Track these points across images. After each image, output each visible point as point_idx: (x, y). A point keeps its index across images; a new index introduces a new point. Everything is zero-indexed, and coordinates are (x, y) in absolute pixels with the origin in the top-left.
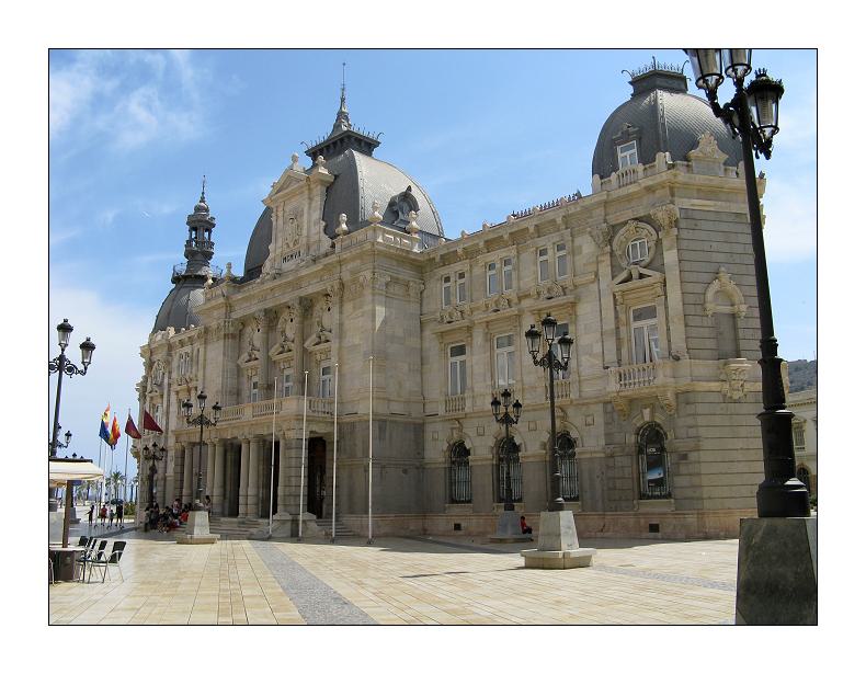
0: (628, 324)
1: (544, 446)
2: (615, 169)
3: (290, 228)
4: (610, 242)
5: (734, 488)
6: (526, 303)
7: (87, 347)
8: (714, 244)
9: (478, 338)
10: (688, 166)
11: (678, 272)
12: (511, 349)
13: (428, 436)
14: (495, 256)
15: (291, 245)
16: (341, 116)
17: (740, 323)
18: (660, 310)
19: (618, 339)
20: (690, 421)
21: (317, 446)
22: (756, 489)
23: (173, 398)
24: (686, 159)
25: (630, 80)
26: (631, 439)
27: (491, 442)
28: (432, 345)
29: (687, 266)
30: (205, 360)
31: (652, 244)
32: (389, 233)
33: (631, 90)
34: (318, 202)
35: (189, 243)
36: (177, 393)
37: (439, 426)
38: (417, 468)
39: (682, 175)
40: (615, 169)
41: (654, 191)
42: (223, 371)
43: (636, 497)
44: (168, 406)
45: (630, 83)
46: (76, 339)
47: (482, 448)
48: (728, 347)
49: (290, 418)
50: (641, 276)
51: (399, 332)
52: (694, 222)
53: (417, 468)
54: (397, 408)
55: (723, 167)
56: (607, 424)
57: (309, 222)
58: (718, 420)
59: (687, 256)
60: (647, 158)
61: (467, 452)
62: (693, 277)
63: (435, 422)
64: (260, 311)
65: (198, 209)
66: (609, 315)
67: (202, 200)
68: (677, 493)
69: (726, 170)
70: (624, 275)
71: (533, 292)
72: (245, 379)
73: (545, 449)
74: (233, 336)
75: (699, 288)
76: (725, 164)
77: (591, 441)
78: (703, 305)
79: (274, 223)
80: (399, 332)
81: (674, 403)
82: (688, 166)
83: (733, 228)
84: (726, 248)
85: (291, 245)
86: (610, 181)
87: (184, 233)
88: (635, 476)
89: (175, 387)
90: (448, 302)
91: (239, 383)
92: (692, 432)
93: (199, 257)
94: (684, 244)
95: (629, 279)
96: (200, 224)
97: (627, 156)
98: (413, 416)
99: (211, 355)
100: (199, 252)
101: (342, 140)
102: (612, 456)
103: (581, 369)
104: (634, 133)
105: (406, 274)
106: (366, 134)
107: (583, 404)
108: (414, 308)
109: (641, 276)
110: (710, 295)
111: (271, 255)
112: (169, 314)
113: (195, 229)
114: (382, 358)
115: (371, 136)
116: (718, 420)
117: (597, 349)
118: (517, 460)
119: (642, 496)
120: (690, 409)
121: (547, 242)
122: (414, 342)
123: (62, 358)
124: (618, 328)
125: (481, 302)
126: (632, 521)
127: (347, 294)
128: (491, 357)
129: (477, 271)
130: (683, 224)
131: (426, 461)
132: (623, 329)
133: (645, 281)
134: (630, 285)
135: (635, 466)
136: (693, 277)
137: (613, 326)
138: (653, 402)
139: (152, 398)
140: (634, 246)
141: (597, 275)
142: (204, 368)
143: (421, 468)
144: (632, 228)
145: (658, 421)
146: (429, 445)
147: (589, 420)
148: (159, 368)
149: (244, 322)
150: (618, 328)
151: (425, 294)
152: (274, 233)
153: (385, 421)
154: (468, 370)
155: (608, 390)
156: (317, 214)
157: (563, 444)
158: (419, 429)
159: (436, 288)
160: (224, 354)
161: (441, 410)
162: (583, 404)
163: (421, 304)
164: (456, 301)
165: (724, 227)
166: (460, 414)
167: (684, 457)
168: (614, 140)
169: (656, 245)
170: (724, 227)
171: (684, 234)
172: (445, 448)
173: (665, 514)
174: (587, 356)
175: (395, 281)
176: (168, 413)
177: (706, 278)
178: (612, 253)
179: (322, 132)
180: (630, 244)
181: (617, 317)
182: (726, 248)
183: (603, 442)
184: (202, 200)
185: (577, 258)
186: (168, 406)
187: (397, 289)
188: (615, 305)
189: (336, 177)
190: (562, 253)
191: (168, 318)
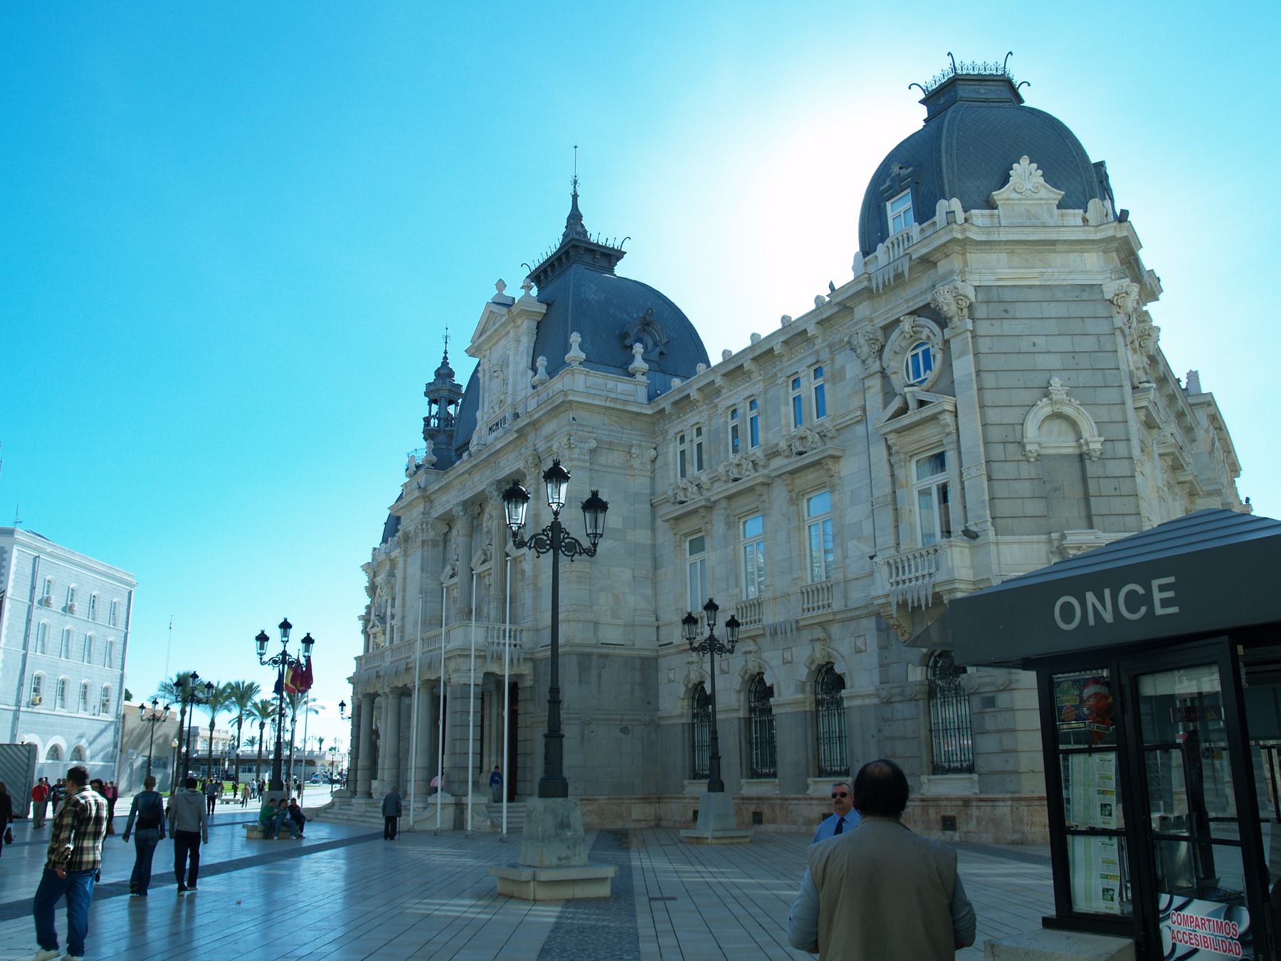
4: (881, 357)
6: (776, 463)
7: (308, 641)
8: (1039, 341)
13: (662, 677)
15: (497, 410)
16: (575, 217)
17: (1091, 469)
22: (911, 796)
24: (991, 205)
25: (923, 96)
27: (803, 673)
30: (405, 579)
33: (923, 112)
35: (427, 420)
41: (935, 264)
45: (922, 102)
46: (296, 635)
47: (791, 692)
50: (922, 403)
56: (882, 648)
61: (769, 692)
63: (669, 655)
64: (458, 504)
66: (882, 471)
70: (896, 404)
73: (803, 692)
75: (1011, 416)
76: (1059, 207)
84: (1064, 343)
85: (497, 410)
90: (683, 474)
95: (904, 410)
97: (899, 209)
98: (638, 645)
102: (888, 702)
104: (909, 175)
106: (602, 242)
107: (851, 619)
109: (922, 403)
110: (1031, 431)
111: (479, 423)
113: (435, 402)
115: (610, 244)
117: (867, 529)
118: (839, 703)
122: (642, 536)
123: (284, 653)
130: (981, 312)
131: (660, 714)
133: (927, 412)
134: (905, 420)
141: (864, 409)
142: (404, 590)
143: (655, 724)
146: (663, 691)
147: (860, 643)
148: (383, 593)
149: (448, 520)
151: (659, 463)
153: (589, 655)
155: (874, 594)
160: (422, 569)
162: (851, 619)
163: (653, 479)
164: (692, 470)
167: (990, 702)
171: (983, 328)
174: (854, 542)
177: (1026, 397)
178: (883, 372)
182: (1064, 343)
183: (876, 679)
189: (549, 305)
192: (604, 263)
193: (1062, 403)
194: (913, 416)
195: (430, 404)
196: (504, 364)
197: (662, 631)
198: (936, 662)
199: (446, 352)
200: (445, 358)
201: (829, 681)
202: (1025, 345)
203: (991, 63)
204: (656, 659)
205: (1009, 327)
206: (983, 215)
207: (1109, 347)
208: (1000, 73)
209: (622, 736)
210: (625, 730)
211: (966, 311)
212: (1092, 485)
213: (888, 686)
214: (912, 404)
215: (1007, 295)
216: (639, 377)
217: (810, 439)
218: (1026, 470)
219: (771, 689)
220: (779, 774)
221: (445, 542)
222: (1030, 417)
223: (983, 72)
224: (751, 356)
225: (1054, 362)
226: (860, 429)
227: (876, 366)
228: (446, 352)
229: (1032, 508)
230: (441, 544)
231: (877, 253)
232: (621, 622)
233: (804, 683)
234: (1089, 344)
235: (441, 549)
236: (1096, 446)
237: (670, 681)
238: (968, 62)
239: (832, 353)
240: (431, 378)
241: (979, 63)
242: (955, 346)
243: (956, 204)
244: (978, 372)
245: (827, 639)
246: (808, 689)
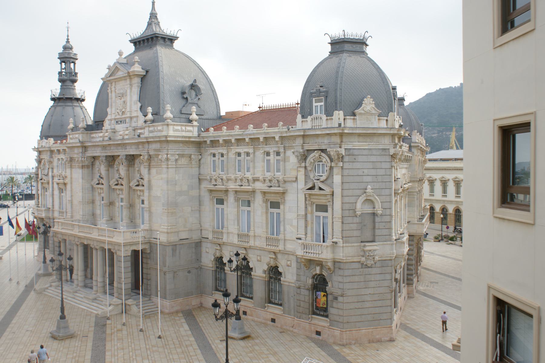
0: (312, 213)
1: (265, 272)
2: (311, 114)
3: (119, 102)
4: (305, 159)
5: (378, 286)
8: (366, 171)
9: (231, 198)
10: (354, 119)
11: (340, 190)
12: (248, 209)
13: (204, 249)
14: (242, 149)
16: (153, 16)
17: (377, 219)
18: (330, 209)
19: (306, 221)
20: (340, 279)
21: (135, 253)
23: (56, 186)
24: (354, 114)
25: (330, 41)
26: (310, 281)
28: (206, 197)
29: (346, 186)
31: (328, 168)
32: (177, 125)
33: (329, 48)
34: (136, 90)
35: (60, 73)
36: (58, 184)
37: (209, 245)
38: (197, 269)
39: (350, 123)
40: (311, 114)
42: (82, 189)
43: (311, 313)
44: (53, 191)
48: (368, 235)
49: (122, 238)
51: (185, 188)
52: (354, 157)
53: (197, 269)
54: (184, 235)
55: (377, 118)
57: (131, 100)
58: (356, 279)
59: (346, 179)
60: (329, 113)
62: (350, 193)
65: (65, 48)
67: (68, 41)
68: (330, 316)
69: (379, 119)
70: (310, 185)
71: (261, 178)
72: (97, 194)
73: (265, 274)
74: (88, 167)
75: (352, 200)
77: (289, 276)
78: (354, 211)
79: (110, 95)
80: (185, 188)
81: (332, 268)
82: (354, 119)
83: (379, 159)
84: (373, 172)
86: (307, 121)
87: (57, 66)
88: (311, 302)
89: (56, 180)
91: (93, 196)
92: (341, 286)
93: (68, 83)
94: (346, 172)
96: (67, 57)
99: (75, 176)
100: (68, 79)
101: (152, 38)
102: (299, 288)
103: (286, 232)
104: (324, 92)
105: (191, 150)
108: (195, 171)
109: (320, 189)
110: (359, 206)
112: (50, 125)
114: (172, 207)
116: (356, 279)
118: (280, 280)
119: (314, 313)
120: (341, 272)
121: (271, 149)
124: (306, 214)
125: (233, 177)
126: (307, 326)
127: (153, 163)
128: (238, 212)
129: (232, 155)
131: (202, 264)
132: (309, 216)
133: (322, 192)
134: (312, 192)
135: (311, 296)
136: (350, 193)
137: (303, 213)
138: (320, 264)
139: (42, 183)
140: (319, 165)
143: (200, 268)
144: (317, 155)
145: (323, 273)
146: (204, 255)
150: (306, 214)
151: (202, 161)
152: (110, 100)
153: (176, 245)
154: (225, 216)
156: (136, 97)
157: (274, 273)
158: (198, 245)
159: (208, 159)
160: (83, 178)
161: (210, 237)
165: (373, 159)
166: (220, 241)
167: (336, 298)
168: (312, 93)
169: (330, 169)
170: (373, 159)
171: (346, 166)
172: (212, 260)
173: (324, 327)
175: (181, 156)
176: (53, 195)
177: (358, 192)
178: (305, 167)
179: (139, 29)
180: (317, 163)
181: (306, 208)
182: (373, 172)
183: (295, 278)
184: (68, 41)
185: (287, 164)
186: (53, 191)
187: (183, 161)
188: (306, 200)
189: (147, 72)
190: (278, 158)
191: (49, 128)
192: (168, 43)
193: (370, 196)
194: (316, 191)
195: (61, 63)
196: (122, 95)
197: (203, 231)
198: (317, 278)
199: (68, 36)
200: (68, 39)
201: (274, 273)
202: (360, 172)
203: (359, 33)
204: (201, 242)
205: (357, 165)
206: (351, 119)
207: (388, 213)
208: (362, 38)
209: (188, 274)
210: (189, 272)
211: (340, 159)
212: (377, 225)
213: (299, 282)
214: (317, 187)
215: (356, 152)
216: (195, 123)
217: (273, 181)
218: (356, 220)
219: (252, 269)
220: (254, 298)
221: (92, 167)
222: (359, 201)
223: (355, 37)
224: (249, 137)
225: (369, 179)
226: (295, 185)
227: (303, 165)
228: (68, 36)
229: (357, 233)
230: (91, 166)
231: (307, 119)
232: (187, 229)
233: (265, 271)
234: (382, 172)
235: (91, 168)
236: (380, 212)
237: (207, 252)
238: (350, 33)
239: (284, 149)
240: (61, 50)
241: (354, 33)
242: (335, 170)
243: (341, 113)
244: (342, 183)
245: (276, 259)
246: (267, 273)
